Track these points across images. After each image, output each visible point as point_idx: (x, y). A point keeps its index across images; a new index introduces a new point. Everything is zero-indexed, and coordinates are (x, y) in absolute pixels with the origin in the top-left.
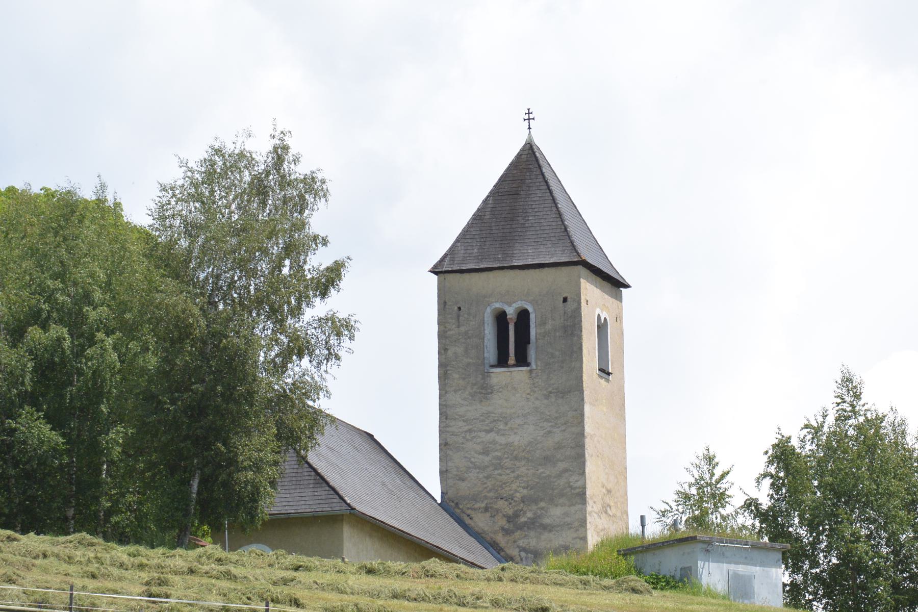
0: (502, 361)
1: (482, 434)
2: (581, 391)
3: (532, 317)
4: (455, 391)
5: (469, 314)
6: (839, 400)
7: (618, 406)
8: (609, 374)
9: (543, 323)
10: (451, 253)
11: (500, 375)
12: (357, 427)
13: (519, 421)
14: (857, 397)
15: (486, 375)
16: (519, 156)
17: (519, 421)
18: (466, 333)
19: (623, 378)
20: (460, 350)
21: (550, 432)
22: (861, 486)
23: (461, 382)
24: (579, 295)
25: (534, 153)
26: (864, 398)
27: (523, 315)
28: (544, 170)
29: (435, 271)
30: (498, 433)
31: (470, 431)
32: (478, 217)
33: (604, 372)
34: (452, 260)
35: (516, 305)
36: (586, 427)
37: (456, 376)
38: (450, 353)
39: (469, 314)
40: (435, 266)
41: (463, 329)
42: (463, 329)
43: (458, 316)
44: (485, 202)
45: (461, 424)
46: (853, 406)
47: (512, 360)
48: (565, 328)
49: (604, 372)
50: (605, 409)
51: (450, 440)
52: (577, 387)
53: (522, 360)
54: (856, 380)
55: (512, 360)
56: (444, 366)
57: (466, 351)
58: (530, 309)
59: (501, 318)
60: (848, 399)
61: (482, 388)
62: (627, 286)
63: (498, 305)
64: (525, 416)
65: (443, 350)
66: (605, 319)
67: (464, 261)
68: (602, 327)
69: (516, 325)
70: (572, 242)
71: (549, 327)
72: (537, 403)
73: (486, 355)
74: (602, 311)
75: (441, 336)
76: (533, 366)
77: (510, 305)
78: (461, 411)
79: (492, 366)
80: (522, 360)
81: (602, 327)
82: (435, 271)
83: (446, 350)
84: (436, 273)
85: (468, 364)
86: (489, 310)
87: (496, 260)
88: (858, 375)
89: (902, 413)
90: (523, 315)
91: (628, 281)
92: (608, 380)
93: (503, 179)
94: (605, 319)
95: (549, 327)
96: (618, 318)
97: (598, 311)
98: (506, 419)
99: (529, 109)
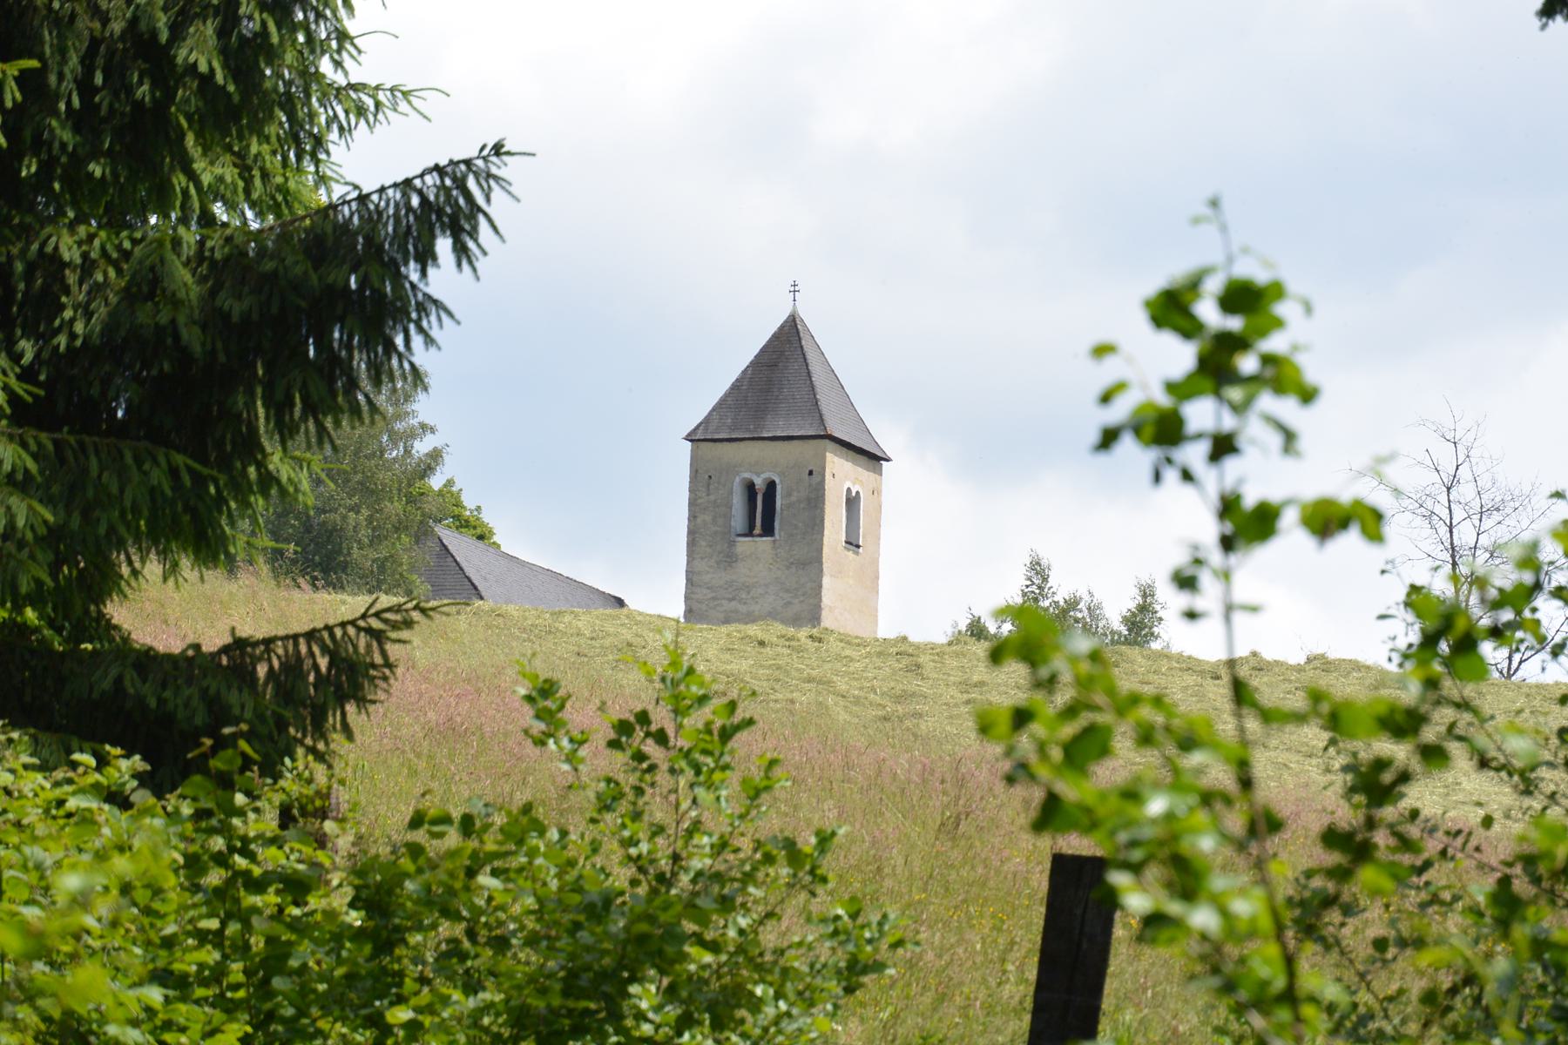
0: (749, 533)
1: (724, 602)
2: (821, 563)
3: (779, 488)
4: (702, 558)
5: (719, 483)
6: (1029, 583)
7: (871, 580)
8: (858, 546)
9: (789, 495)
10: (706, 421)
11: (744, 545)
12: (607, 591)
13: (760, 591)
14: (1045, 580)
15: (732, 544)
16: (782, 327)
17: (760, 591)
18: (715, 501)
19: (878, 552)
20: (708, 518)
21: (790, 603)
22: (82, 565)
23: (708, 550)
24: (824, 469)
25: (796, 325)
26: (1051, 582)
27: (771, 486)
28: (803, 343)
29: (690, 438)
30: (740, 602)
31: (714, 599)
32: (736, 387)
33: (852, 544)
34: (706, 429)
35: (764, 476)
36: (824, 599)
37: (704, 543)
38: (699, 520)
39: (719, 483)
40: (689, 435)
41: (712, 498)
42: (712, 498)
43: (709, 485)
44: (744, 372)
45: (705, 591)
46: (1039, 587)
47: (757, 530)
48: (809, 500)
49: (852, 544)
50: (851, 582)
51: (695, 606)
52: (817, 560)
53: (768, 530)
54: (1044, 562)
55: (757, 530)
56: (692, 534)
57: (714, 520)
58: (777, 481)
59: (750, 488)
60: (1037, 582)
61: (728, 556)
62: (888, 460)
63: (747, 475)
64: (766, 586)
65: (692, 517)
66: (858, 493)
67: (717, 430)
68: (852, 502)
69: (764, 495)
70: (821, 416)
71: (793, 499)
72: (779, 573)
73: (733, 524)
74: (854, 484)
75: (692, 503)
76: (777, 536)
77: (758, 475)
78: (707, 578)
79: (739, 535)
80: (768, 530)
81: (852, 502)
82: (690, 438)
83: (695, 517)
84: (691, 441)
85: (716, 533)
86: (737, 479)
87: (748, 430)
88: (1046, 558)
89: (1098, 597)
90: (771, 486)
91: (889, 454)
92: (857, 553)
93: (763, 350)
94: (858, 493)
95: (793, 499)
96: (876, 492)
97: (848, 484)
98: (748, 588)
99: (1196, 221)
